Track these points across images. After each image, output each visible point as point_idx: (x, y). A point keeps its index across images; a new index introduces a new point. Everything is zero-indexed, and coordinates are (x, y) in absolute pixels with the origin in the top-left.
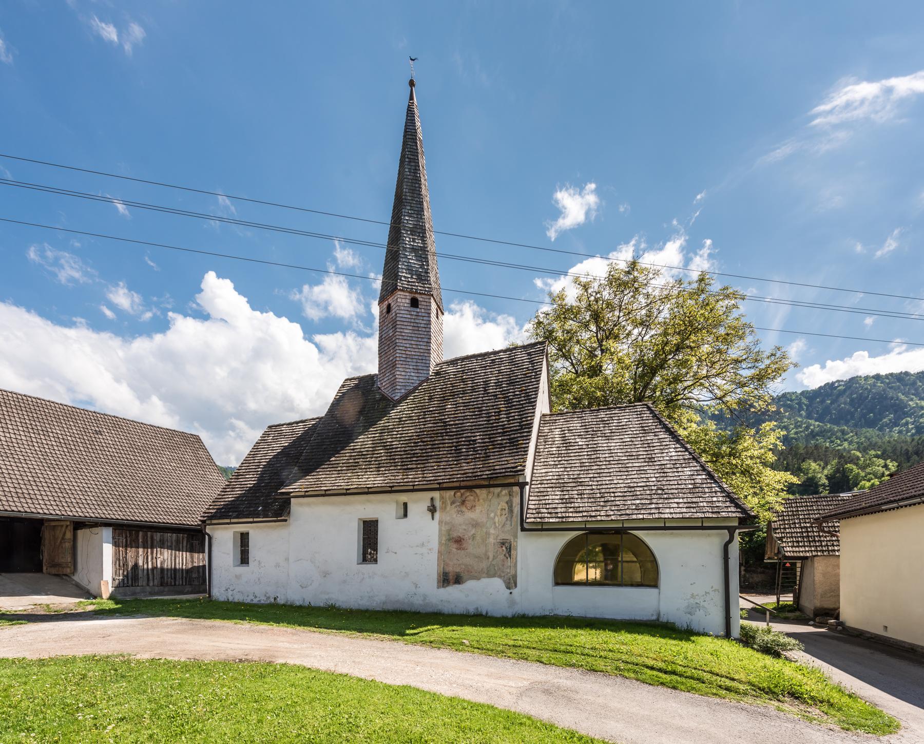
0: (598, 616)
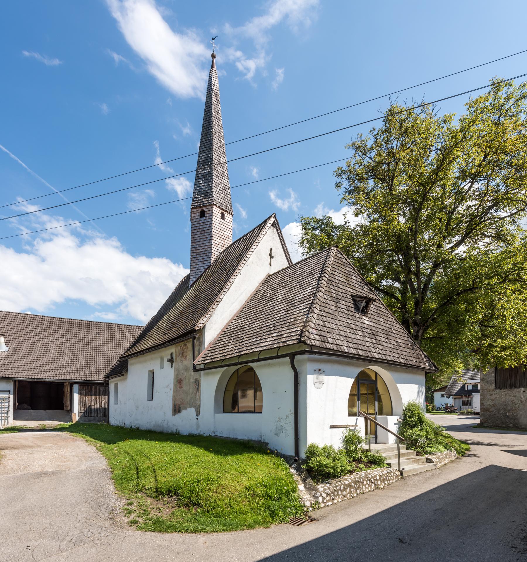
0: (231, 436)
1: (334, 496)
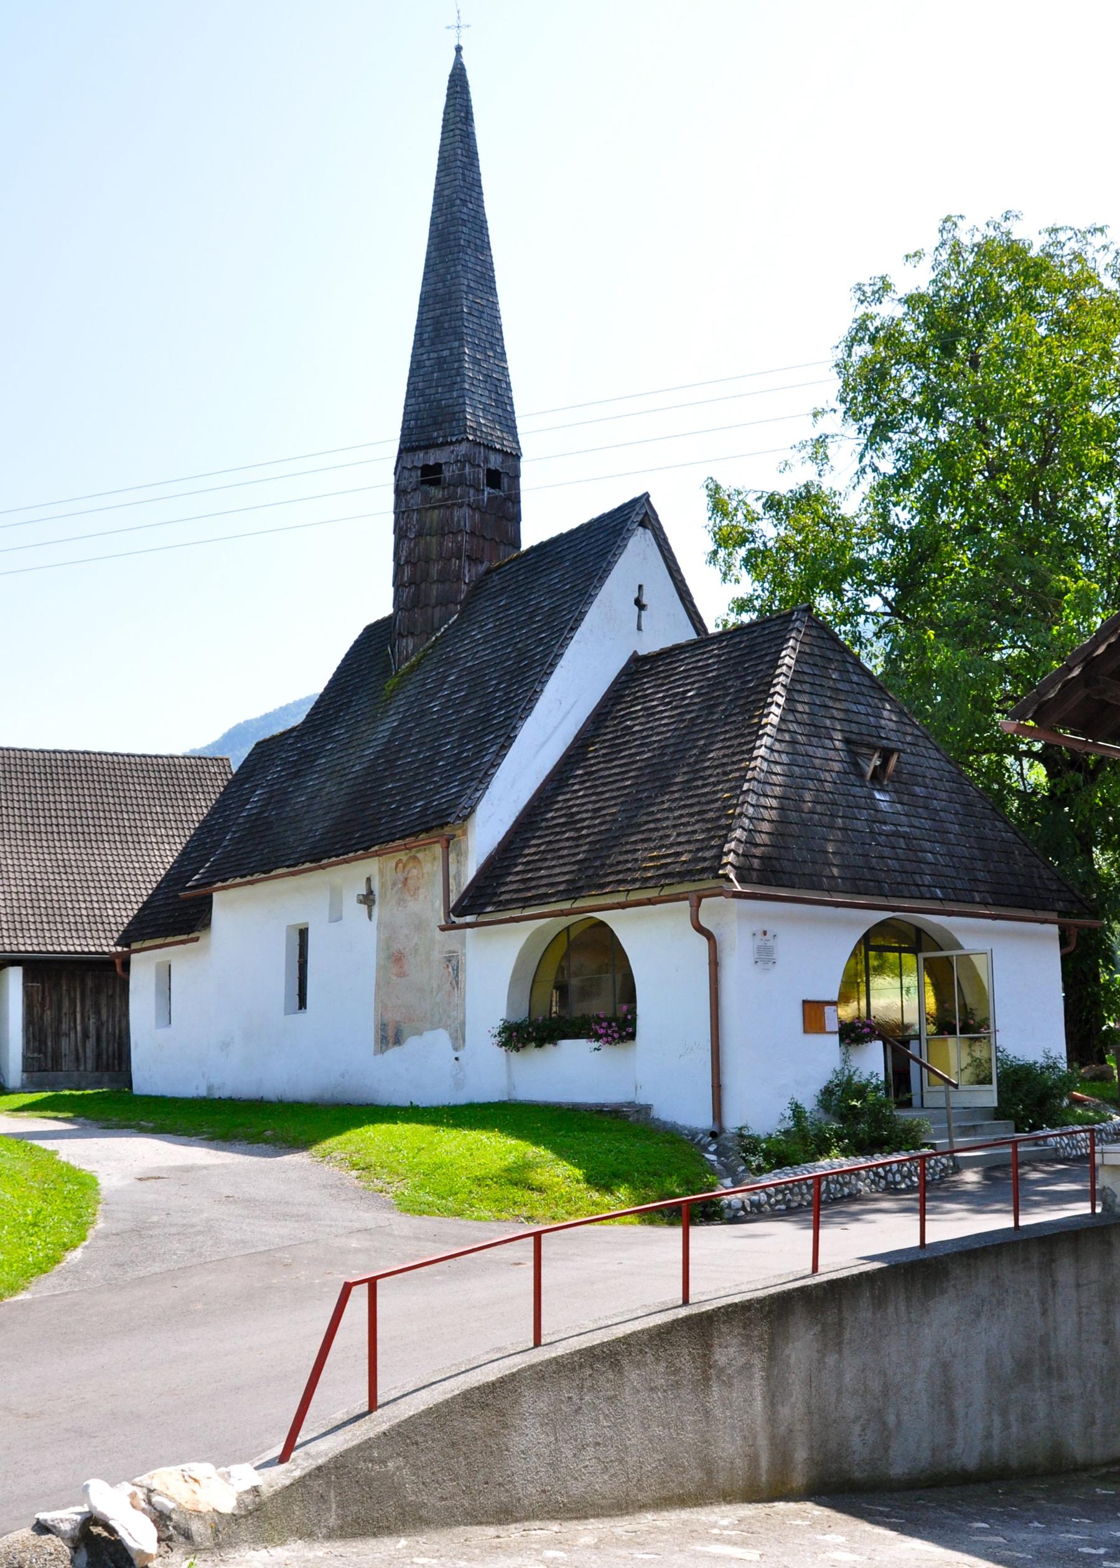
1: (791, 1193)
